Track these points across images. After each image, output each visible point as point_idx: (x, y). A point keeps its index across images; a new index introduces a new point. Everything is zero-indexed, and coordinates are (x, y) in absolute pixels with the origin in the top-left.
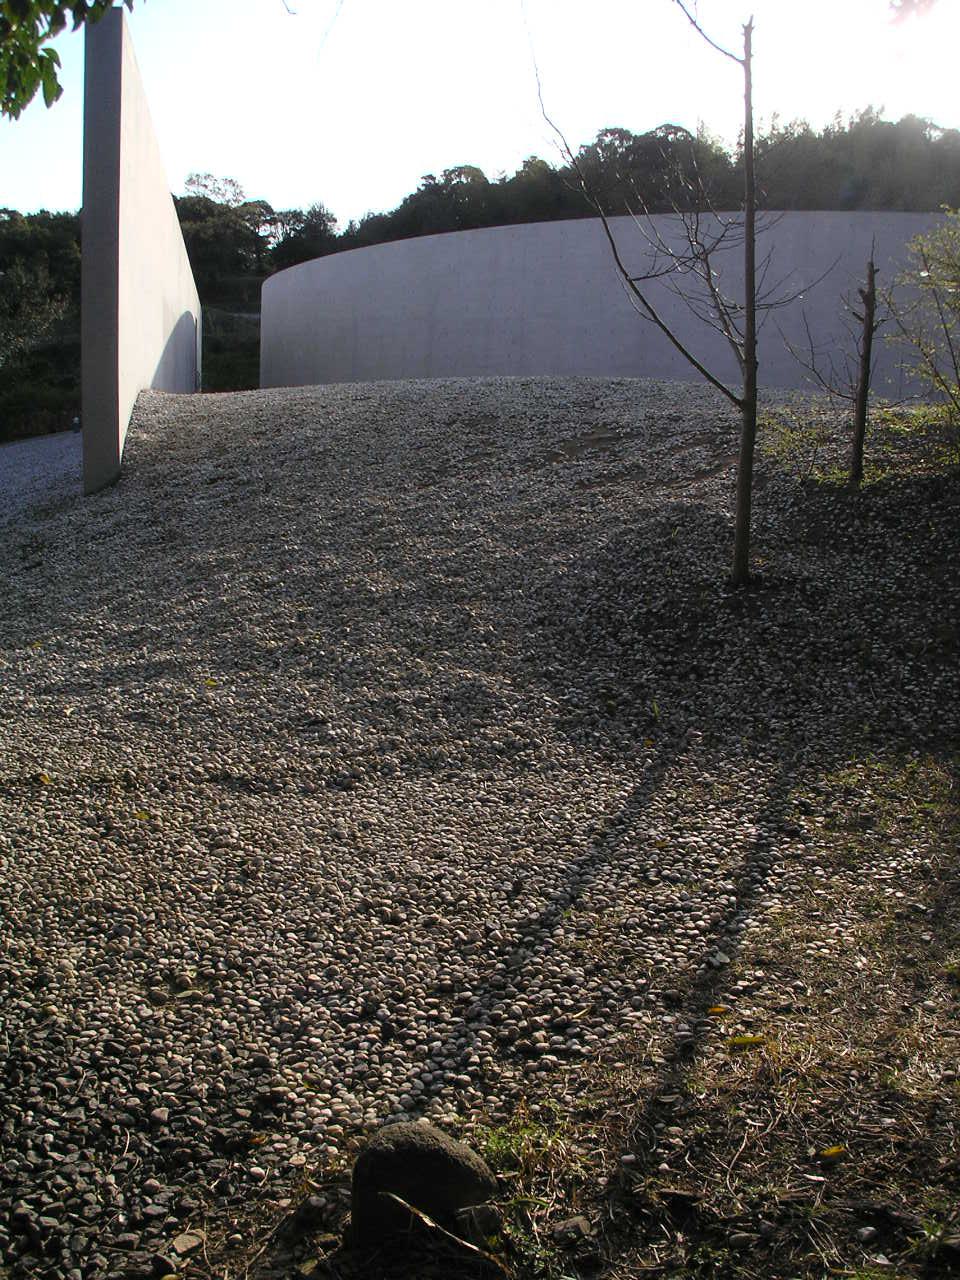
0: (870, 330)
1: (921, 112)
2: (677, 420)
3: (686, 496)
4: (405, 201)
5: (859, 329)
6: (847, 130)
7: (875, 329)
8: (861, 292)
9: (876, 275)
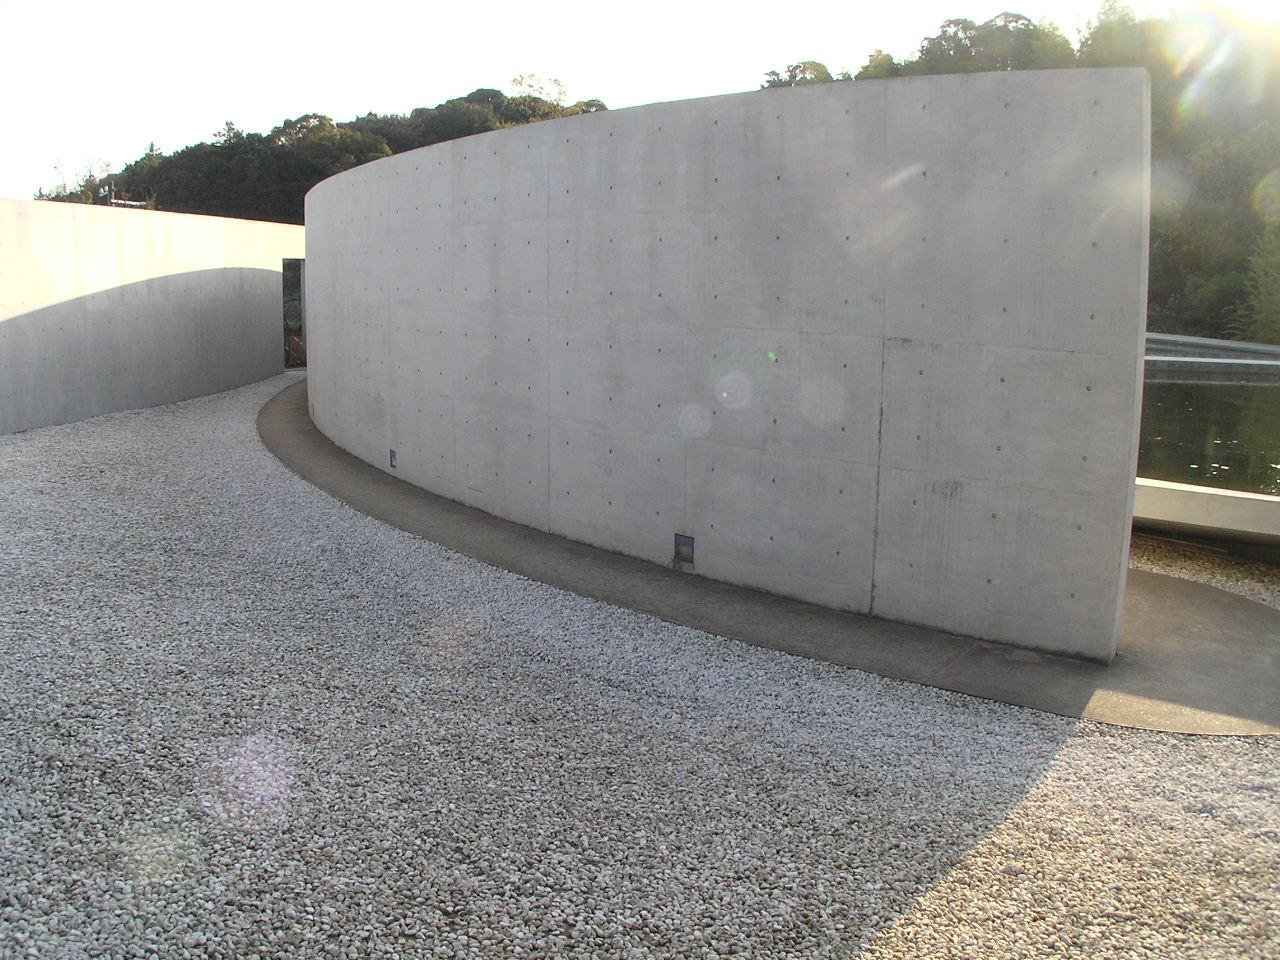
1: (258, 132)
4: (129, 168)
9: (705, 563)
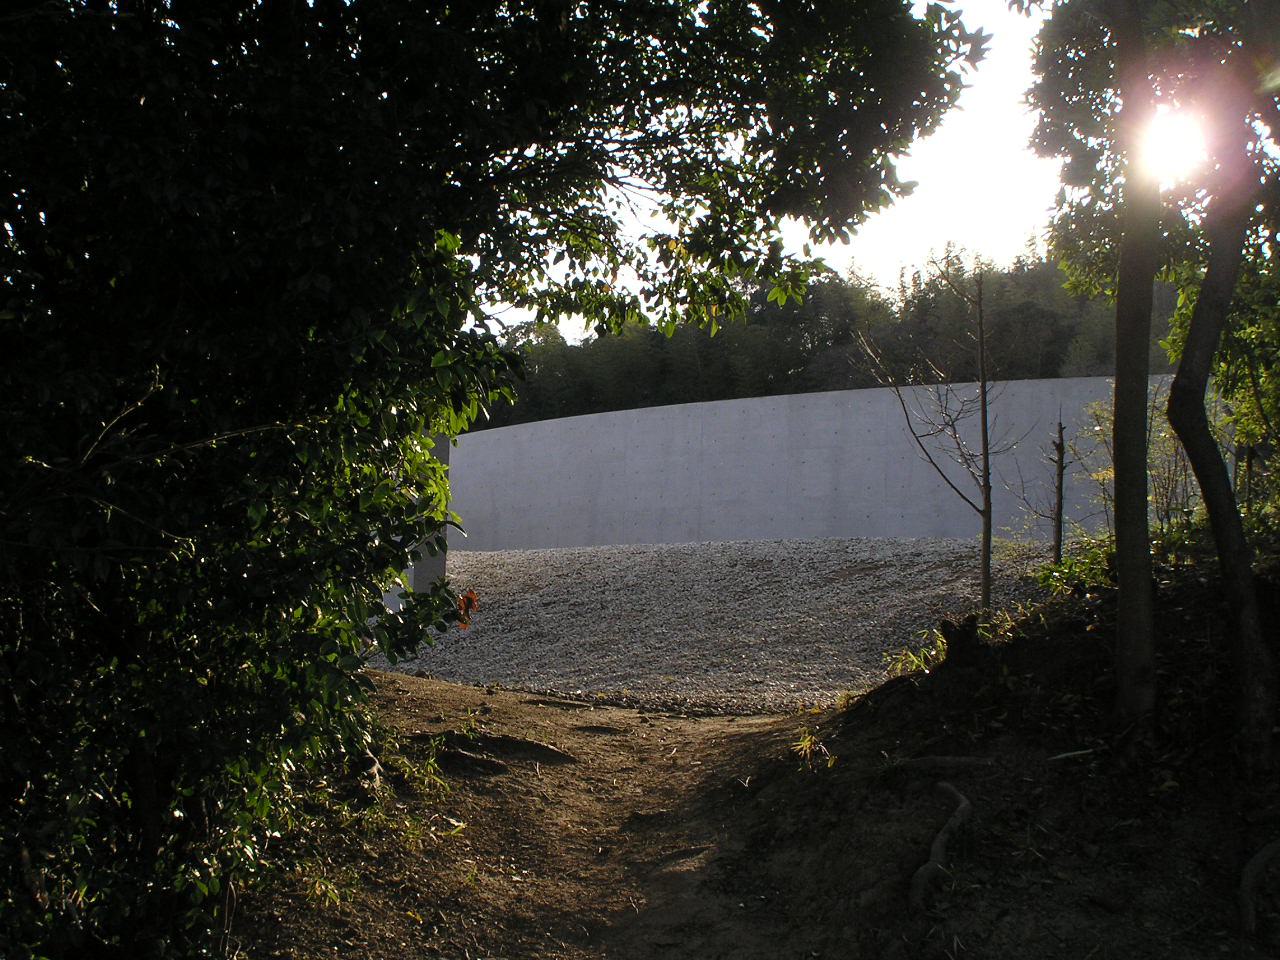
0: (1061, 468)
2: (919, 555)
3: (942, 590)
5: (1054, 468)
6: (1044, 261)
7: (1065, 468)
8: (1054, 442)
